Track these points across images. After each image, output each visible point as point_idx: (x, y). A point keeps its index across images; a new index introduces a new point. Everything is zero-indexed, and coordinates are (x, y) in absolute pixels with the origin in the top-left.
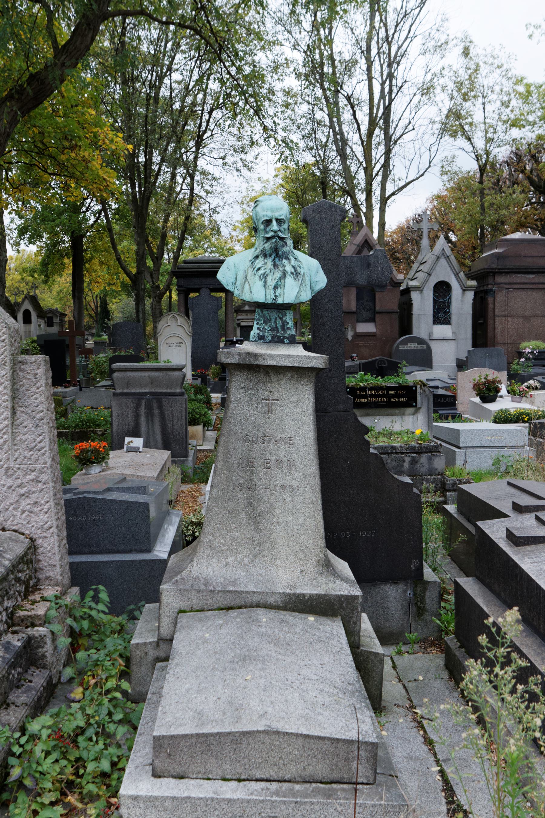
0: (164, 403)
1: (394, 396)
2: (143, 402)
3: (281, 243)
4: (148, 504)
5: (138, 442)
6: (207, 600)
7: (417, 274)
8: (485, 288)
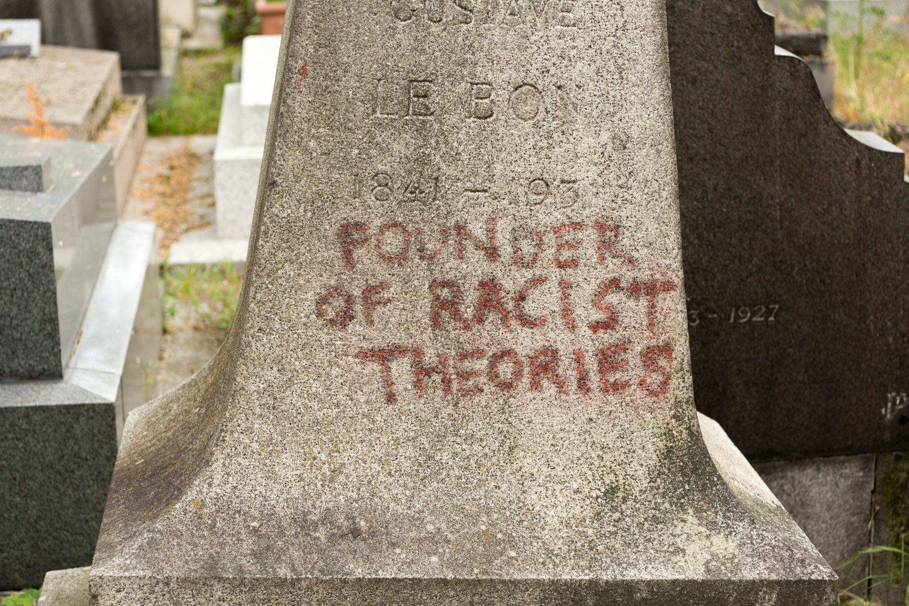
4: (47, 227)
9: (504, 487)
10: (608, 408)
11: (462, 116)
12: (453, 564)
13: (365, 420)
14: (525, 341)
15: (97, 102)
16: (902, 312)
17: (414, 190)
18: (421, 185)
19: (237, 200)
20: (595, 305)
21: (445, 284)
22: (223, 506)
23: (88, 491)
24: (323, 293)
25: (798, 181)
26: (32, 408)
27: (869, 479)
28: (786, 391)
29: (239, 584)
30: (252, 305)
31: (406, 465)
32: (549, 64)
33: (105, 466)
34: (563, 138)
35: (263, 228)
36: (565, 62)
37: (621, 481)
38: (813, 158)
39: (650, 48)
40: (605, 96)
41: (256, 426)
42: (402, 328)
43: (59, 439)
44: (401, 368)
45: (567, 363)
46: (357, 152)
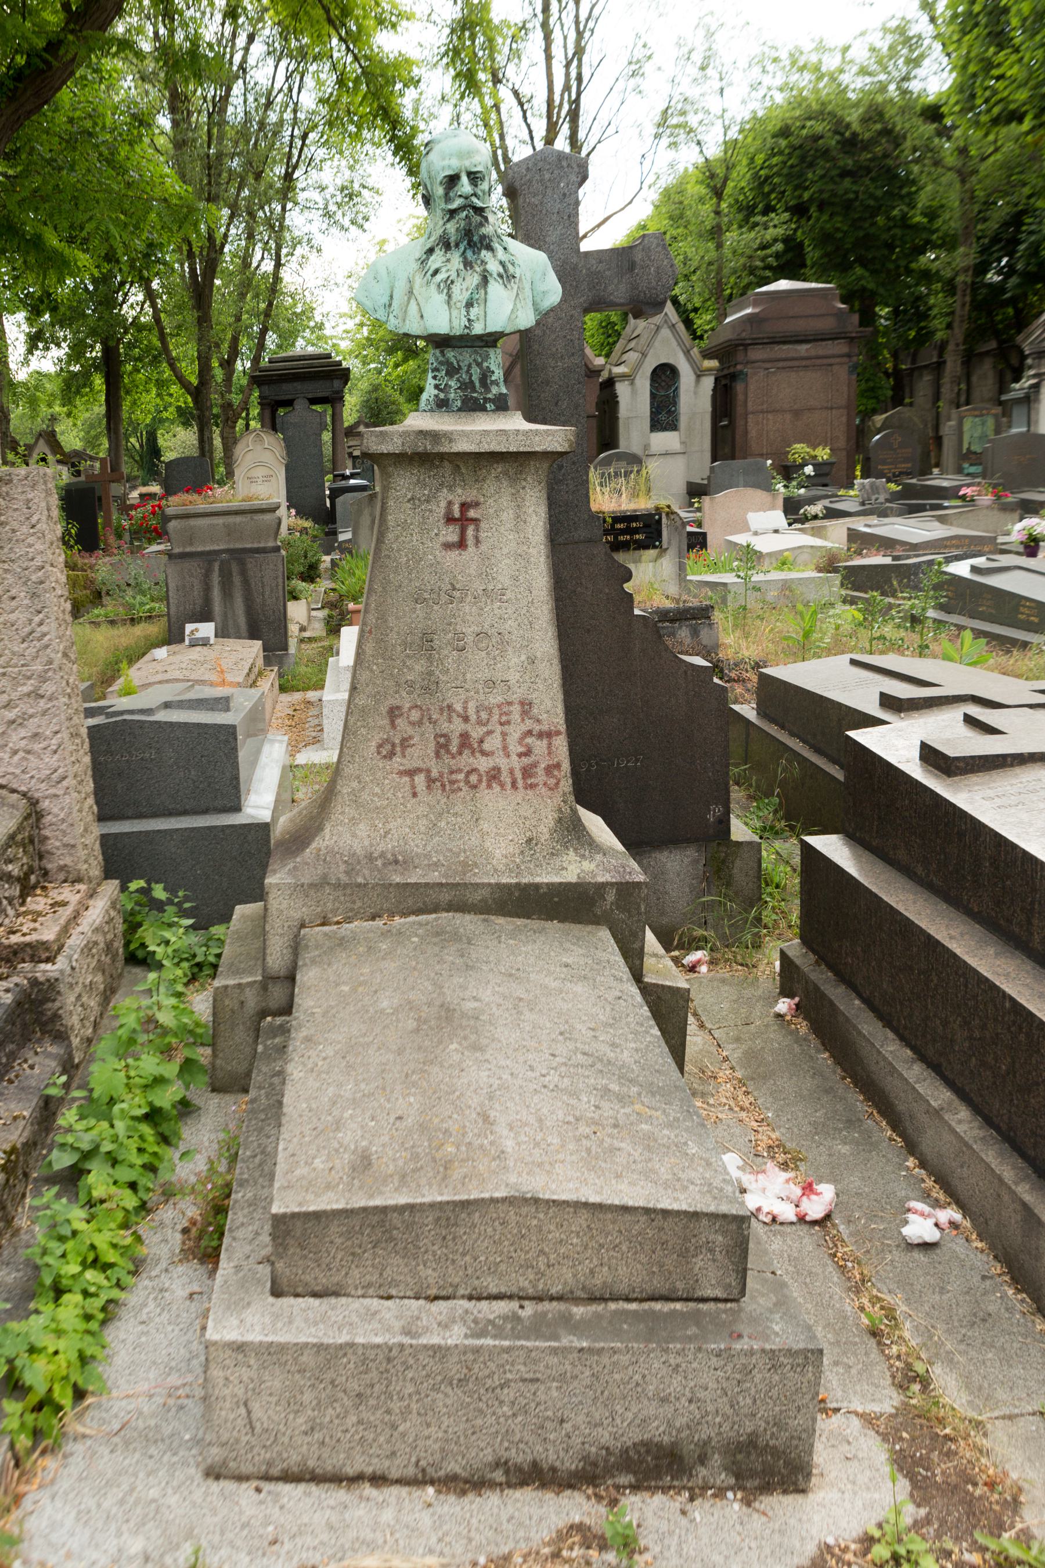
0: (249, 566)
1: (623, 532)
2: (216, 566)
3: (478, 218)
5: (206, 629)
6: (354, 902)
7: (625, 357)
8: (732, 370)
12: (446, 876)
14: (483, 764)
17: (426, 689)
18: (430, 686)
19: (333, 726)
21: (442, 736)
22: (330, 851)
29: (338, 886)
31: (423, 829)
40: (523, 637)
44: (420, 780)
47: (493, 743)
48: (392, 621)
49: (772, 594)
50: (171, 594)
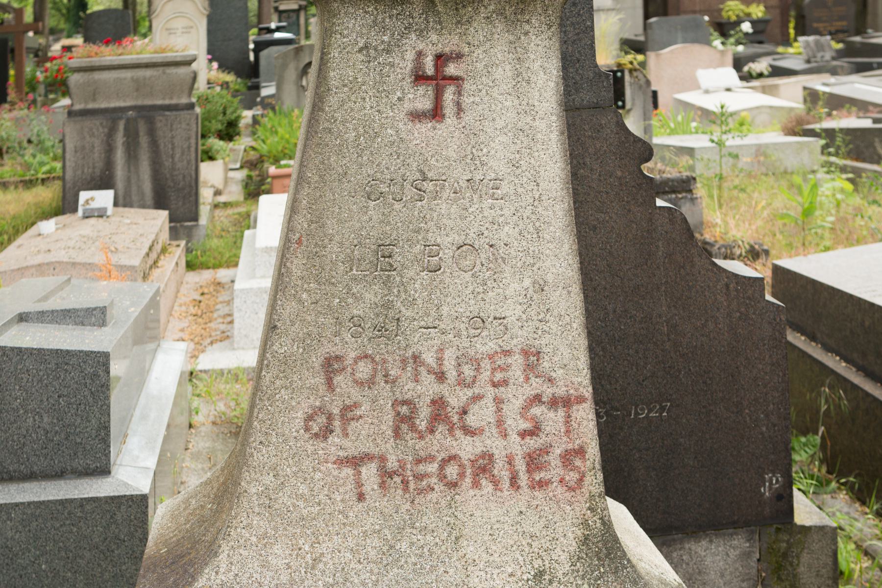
0: (159, 125)
2: (121, 125)
4: (106, 356)
5: (104, 198)
9: (451, 571)
10: (535, 503)
11: (418, 271)
13: (340, 516)
14: (467, 448)
15: (150, 249)
16: (772, 406)
17: (381, 329)
18: (387, 325)
19: (250, 321)
20: (522, 416)
21: (405, 402)
23: (124, 567)
24: (310, 412)
25: (680, 303)
26: (85, 499)
27: (754, 549)
28: (679, 474)
30: (255, 423)
31: (373, 554)
32: (483, 228)
33: (138, 546)
34: (495, 285)
35: (265, 362)
36: (496, 227)
37: (547, 566)
38: (691, 284)
39: (560, 214)
40: (526, 251)
41: (255, 522)
42: (371, 439)
43: (104, 524)
44: (369, 471)
45: (501, 465)
46: (338, 300)
47: (481, 415)
48: (332, 227)
49: (745, 160)
50: (68, 156)
